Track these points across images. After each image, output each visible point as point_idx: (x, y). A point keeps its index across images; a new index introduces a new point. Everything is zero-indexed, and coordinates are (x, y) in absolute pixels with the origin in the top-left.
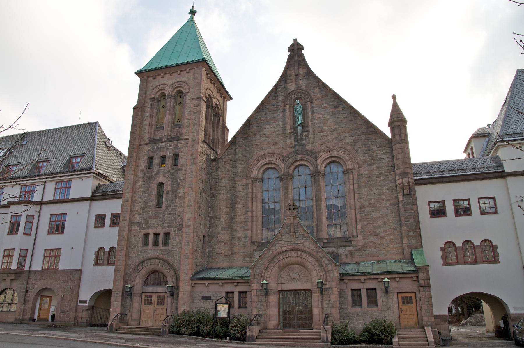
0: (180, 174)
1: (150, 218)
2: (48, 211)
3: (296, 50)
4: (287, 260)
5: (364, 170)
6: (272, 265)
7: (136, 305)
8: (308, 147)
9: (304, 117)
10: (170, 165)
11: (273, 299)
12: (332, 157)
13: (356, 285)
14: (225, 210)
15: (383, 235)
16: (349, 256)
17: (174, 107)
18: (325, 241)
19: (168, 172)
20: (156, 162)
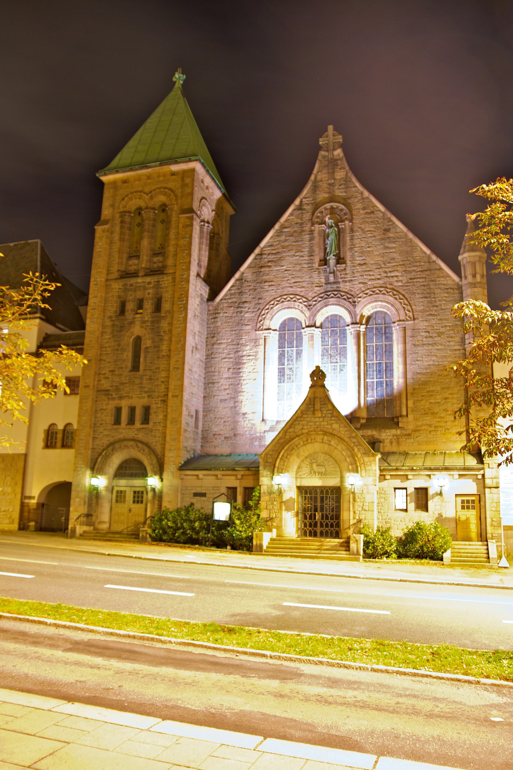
1: (122, 384)
16: (394, 444)
19: (147, 321)
20: (130, 306)
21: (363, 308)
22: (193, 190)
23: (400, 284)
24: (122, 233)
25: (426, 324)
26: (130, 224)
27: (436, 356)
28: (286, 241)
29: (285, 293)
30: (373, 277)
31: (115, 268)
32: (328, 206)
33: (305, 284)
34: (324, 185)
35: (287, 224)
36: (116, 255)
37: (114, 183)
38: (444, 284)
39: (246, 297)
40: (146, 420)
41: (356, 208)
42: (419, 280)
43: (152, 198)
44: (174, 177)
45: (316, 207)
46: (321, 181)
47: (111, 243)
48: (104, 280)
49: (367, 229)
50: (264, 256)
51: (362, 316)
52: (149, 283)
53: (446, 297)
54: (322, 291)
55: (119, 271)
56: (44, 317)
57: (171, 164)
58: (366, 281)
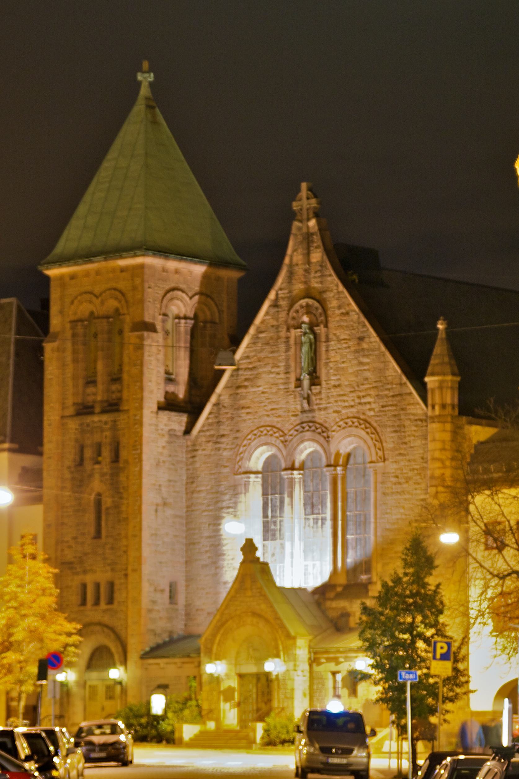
0: (122, 478)
1: (86, 554)
8: (320, 416)
10: (108, 460)
17: (110, 340)
20: (88, 453)
21: (339, 442)
22: (143, 295)
23: (372, 413)
24: (75, 352)
25: (395, 466)
26: (85, 335)
27: (403, 507)
28: (262, 351)
29: (262, 424)
30: (347, 404)
31: (70, 401)
32: (303, 302)
33: (280, 412)
34: (299, 271)
35: (263, 328)
36: (70, 383)
37: (61, 278)
38: (414, 414)
39: (225, 429)
40: (111, 600)
41: (332, 306)
42: (390, 408)
43: (102, 303)
44: (124, 274)
45: (292, 302)
46: (297, 265)
47: (63, 365)
48: (57, 418)
49: (343, 337)
50: (241, 372)
51: (338, 455)
52: (106, 423)
53: (415, 431)
54: (298, 422)
55: (74, 404)
56: (15, 446)
57: (116, 259)
58: (340, 409)
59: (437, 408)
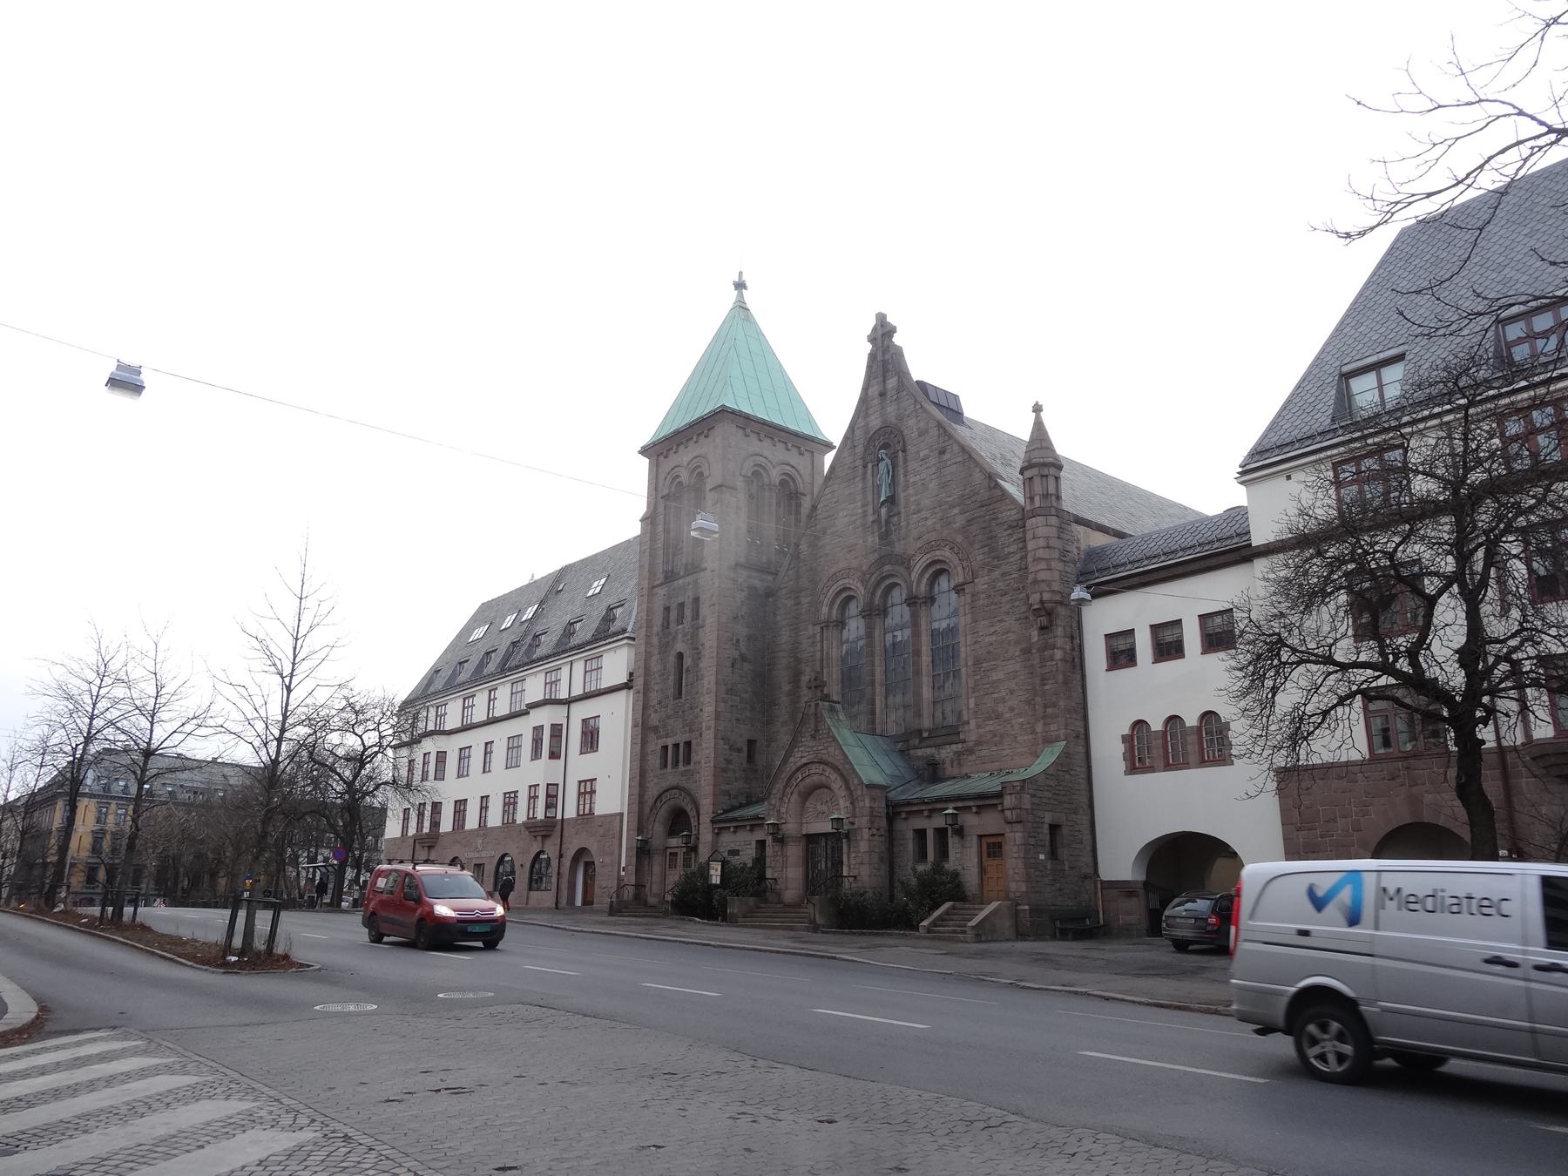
2: (581, 711)
3: (882, 334)
4: (808, 780)
5: (981, 583)
6: (789, 790)
7: (656, 869)
8: (898, 548)
9: (893, 483)
11: (794, 852)
12: (883, 579)
13: (919, 823)
14: (786, 687)
15: (1007, 716)
18: (925, 735)
20: (673, 615)
31: (660, 568)
40: (688, 761)
59: (1037, 499)
